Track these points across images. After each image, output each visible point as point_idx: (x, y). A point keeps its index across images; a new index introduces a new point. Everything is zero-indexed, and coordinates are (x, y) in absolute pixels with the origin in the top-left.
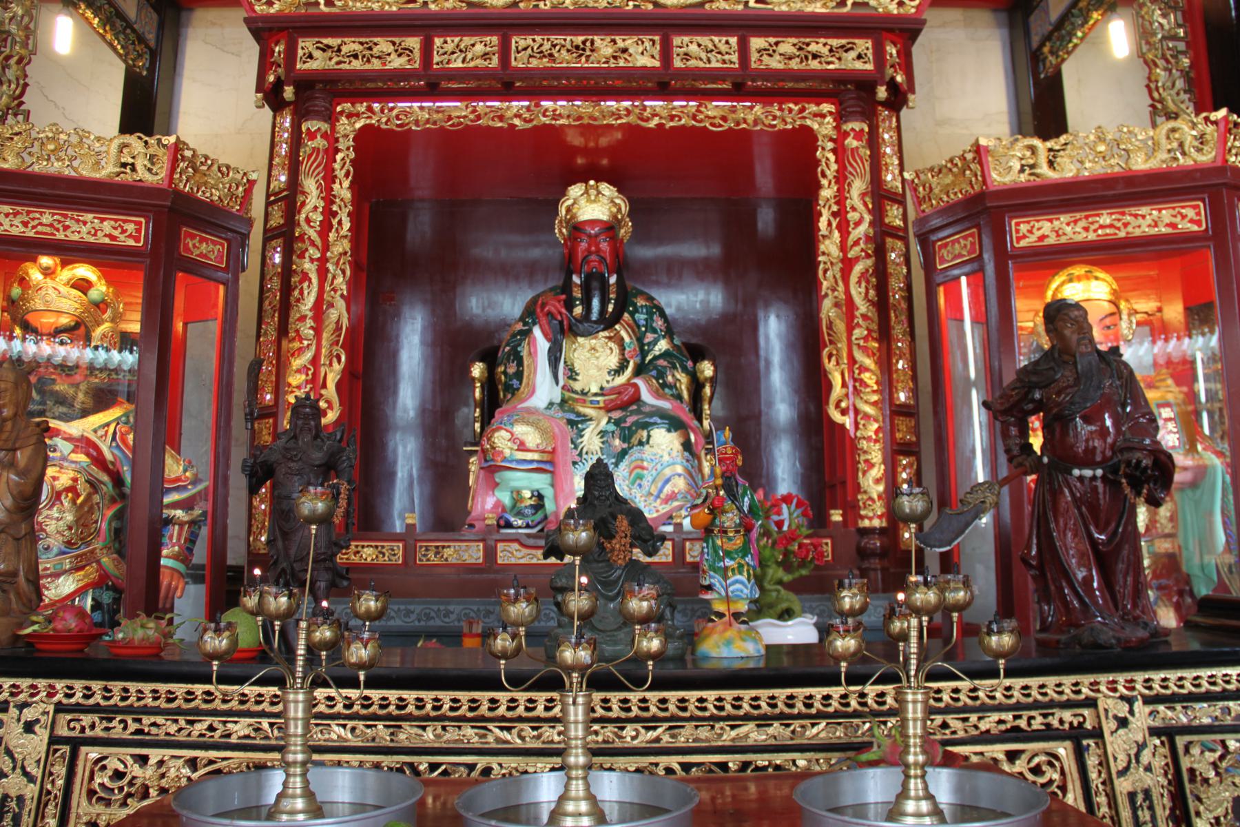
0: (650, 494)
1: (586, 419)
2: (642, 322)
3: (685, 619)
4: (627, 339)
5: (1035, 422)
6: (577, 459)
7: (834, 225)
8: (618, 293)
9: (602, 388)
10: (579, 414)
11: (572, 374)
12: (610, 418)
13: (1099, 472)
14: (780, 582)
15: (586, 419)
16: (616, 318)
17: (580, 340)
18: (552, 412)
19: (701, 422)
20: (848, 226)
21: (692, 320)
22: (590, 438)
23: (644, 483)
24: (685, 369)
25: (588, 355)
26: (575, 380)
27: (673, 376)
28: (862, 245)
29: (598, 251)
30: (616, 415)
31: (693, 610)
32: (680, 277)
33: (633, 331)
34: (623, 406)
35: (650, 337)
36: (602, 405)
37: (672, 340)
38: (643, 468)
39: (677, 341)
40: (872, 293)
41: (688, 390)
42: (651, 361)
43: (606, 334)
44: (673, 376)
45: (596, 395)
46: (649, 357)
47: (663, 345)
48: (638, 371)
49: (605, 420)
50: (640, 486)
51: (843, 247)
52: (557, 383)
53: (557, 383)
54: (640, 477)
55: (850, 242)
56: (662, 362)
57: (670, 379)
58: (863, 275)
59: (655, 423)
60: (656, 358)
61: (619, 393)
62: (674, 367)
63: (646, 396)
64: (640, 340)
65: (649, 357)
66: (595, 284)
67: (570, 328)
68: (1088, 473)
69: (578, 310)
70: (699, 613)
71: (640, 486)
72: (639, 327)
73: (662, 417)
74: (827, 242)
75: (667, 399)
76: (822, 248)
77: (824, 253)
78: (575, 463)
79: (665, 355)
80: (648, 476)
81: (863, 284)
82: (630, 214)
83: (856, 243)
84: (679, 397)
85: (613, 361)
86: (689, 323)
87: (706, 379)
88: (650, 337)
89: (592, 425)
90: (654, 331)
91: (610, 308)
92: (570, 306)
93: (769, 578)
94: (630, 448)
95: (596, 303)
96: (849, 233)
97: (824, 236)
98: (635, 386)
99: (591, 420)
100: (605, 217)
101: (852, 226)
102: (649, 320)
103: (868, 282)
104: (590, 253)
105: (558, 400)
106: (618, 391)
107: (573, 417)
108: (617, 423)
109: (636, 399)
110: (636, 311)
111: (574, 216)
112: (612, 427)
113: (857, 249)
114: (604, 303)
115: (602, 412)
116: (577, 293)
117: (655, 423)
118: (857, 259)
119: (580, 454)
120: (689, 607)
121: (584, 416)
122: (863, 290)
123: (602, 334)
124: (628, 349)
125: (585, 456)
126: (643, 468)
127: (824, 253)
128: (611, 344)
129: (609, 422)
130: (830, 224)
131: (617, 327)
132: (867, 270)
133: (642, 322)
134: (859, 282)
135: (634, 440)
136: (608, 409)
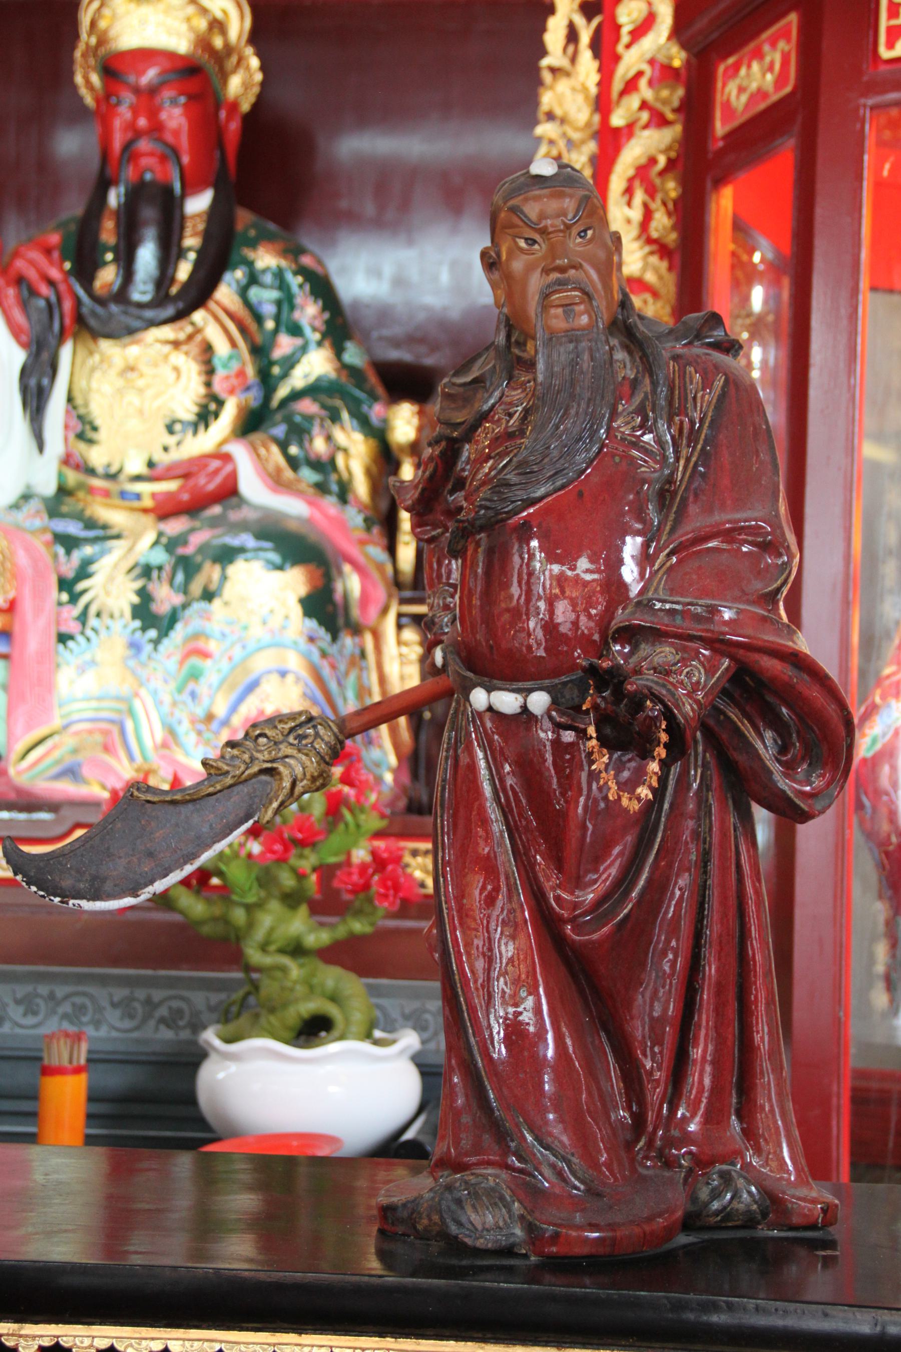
0: (210, 717)
1: (104, 534)
2: (269, 309)
3: (127, 1024)
4: (222, 348)
5: (631, 546)
6: (72, 627)
7: (585, 37)
8: (207, 236)
9: (151, 464)
10: (90, 524)
11: (84, 429)
12: (160, 534)
13: (539, 701)
14: (297, 950)
15: (104, 534)
16: (200, 293)
17: (105, 345)
18: (20, 517)
19: (392, 549)
20: (618, 38)
21: (427, 308)
22: (111, 579)
23: (202, 688)
24: (364, 424)
25: (120, 383)
26: (91, 442)
27: (329, 438)
28: (645, 91)
29: (157, 129)
30: (175, 527)
31: (148, 1002)
32: (405, 205)
33: (243, 329)
34: (191, 506)
35: (285, 344)
36: (148, 503)
37: (338, 351)
38: (206, 655)
39: (353, 355)
40: (661, 221)
41: (368, 472)
42: (285, 402)
43: (167, 332)
44: (329, 438)
45: (138, 478)
46: (282, 392)
47: (316, 364)
48: (251, 423)
49: (150, 537)
50: (193, 695)
51: (603, 104)
52: (41, 447)
53: (41, 447)
54: (195, 676)
55: (617, 85)
56: (307, 406)
57: (319, 445)
58: (642, 172)
59: (241, 550)
60: (296, 396)
61: (186, 476)
62: (335, 417)
63: (253, 487)
64: (260, 351)
65: (282, 392)
66: (149, 213)
67: (79, 319)
68: (507, 701)
69: (108, 276)
70: (163, 1011)
71: (193, 695)
72: (259, 319)
73: (261, 535)
74: (563, 86)
75: (298, 493)
76: (547, 100)
77: (550, 116)
78: (63, 638)
79: (314, 390)
80: (213, 672)
81: (639, 196)
82: (256, 38)
83: (631, 86)
84: (344, 493)
85: (185, 397)
86: (421, 316)
87: (402, 448)
88: (285, 344)
89: (118, 548)
90: (296, 330)
91: (184, 271)
92: (85, 270)
93: (260, 934)
94: (185, 606)
95: (147, 256)
96: (617, 58)
97: (553, 70)
98: (227, 458)
99: (118, 537)
100: (181, 43)
101: (625, 38)
102: (286, 302)
103: (651, 191)
104: (138, 134)
105: (49, 488)
106: (185, 472)
107: (73, 528)
108: (171, 545)
109: (229, 492)
110: (253, 279)
111: (103, 40)
112: (159, 557)
113: (634, 101)
114: (169, 253)
115: (149, 520)
116: (108, 232)
117: (241, 550)
118: (630, 129)
119: (83, 618)
120: (141, 994)
121: (105, 527)
122: (636, 214)
123: (155, 333)
124: (221, 372)
125: (93, 621)
126: (206, 655)
127: (550, 116)
128: (179, 359)
129: (156, 543)
130: (572, 36)
131: (199, 316)
132: (653, 161)
133: (269, 309)
134: (629, 191)
135: (196, 588)
136: (165, 510)
